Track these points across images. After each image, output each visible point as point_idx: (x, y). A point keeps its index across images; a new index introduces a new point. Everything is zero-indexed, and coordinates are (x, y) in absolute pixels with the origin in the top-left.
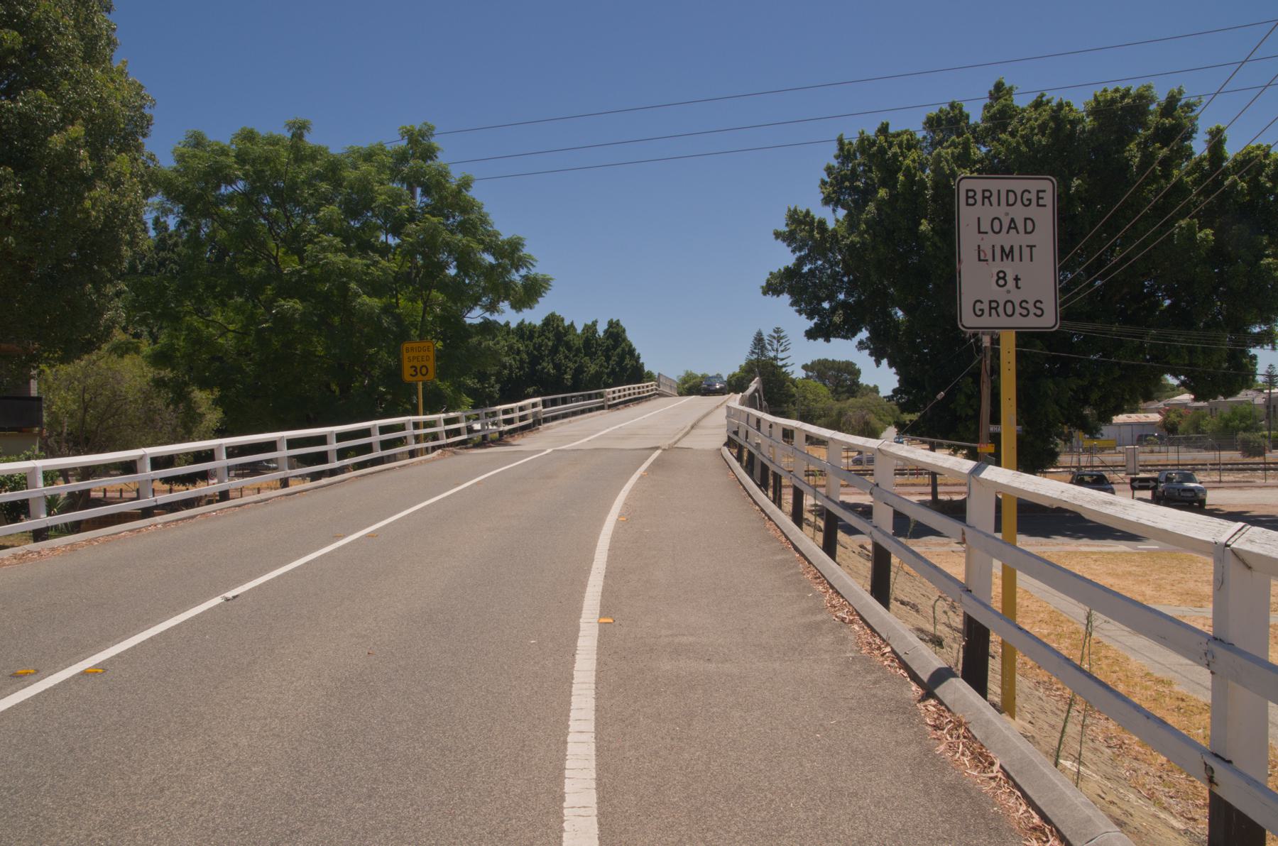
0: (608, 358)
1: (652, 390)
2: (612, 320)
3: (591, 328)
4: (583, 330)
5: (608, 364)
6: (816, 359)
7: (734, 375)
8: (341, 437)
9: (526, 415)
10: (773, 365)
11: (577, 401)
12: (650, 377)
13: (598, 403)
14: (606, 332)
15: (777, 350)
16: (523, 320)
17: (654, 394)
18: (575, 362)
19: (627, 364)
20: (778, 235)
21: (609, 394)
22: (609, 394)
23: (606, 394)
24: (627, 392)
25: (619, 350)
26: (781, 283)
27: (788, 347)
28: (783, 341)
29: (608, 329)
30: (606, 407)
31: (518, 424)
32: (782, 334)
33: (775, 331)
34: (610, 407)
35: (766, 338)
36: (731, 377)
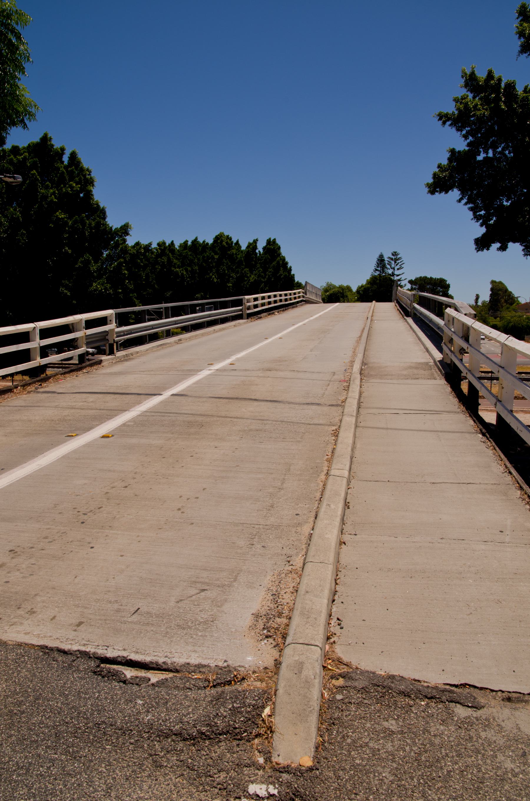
0: (265, 270)
1: (299, 297)
2: (270, 239)
3: (253, 246)
4: (247, 248)
5: (266, 275)
6: (418, 276)
7: (362, 286)
8: (45, 333)
9: (28, 351)
10: (391, 280)
11: (203, 311)
12: (299, 286)
13: (234, 312)
14: (264, 248)
15: (394, 269)
16: (196, 238)
17: (301, 301)
18: (238, 272)
19: (281, 275)
20: (443, 118)
21: (248, 301)
22: (248, 301)
23: (245, 301)
24: (272, 299)
25: (274, 263)
26: (451, 176)
27: (403, 266)
28: (399, 261)
29: (266, 246)
30: (245, 316)
31: (279, 304)
32: (398, 256)
33: (393, 255)
34: (249, 316)
35: (386, 259)
36: (360, 288)
